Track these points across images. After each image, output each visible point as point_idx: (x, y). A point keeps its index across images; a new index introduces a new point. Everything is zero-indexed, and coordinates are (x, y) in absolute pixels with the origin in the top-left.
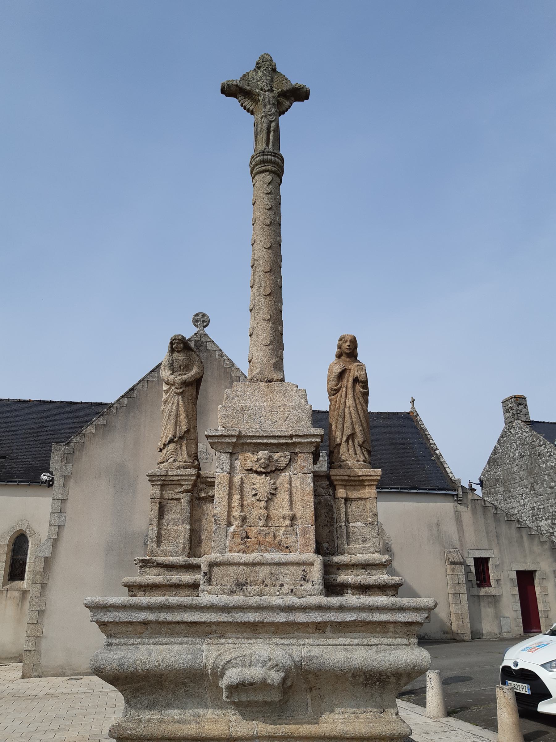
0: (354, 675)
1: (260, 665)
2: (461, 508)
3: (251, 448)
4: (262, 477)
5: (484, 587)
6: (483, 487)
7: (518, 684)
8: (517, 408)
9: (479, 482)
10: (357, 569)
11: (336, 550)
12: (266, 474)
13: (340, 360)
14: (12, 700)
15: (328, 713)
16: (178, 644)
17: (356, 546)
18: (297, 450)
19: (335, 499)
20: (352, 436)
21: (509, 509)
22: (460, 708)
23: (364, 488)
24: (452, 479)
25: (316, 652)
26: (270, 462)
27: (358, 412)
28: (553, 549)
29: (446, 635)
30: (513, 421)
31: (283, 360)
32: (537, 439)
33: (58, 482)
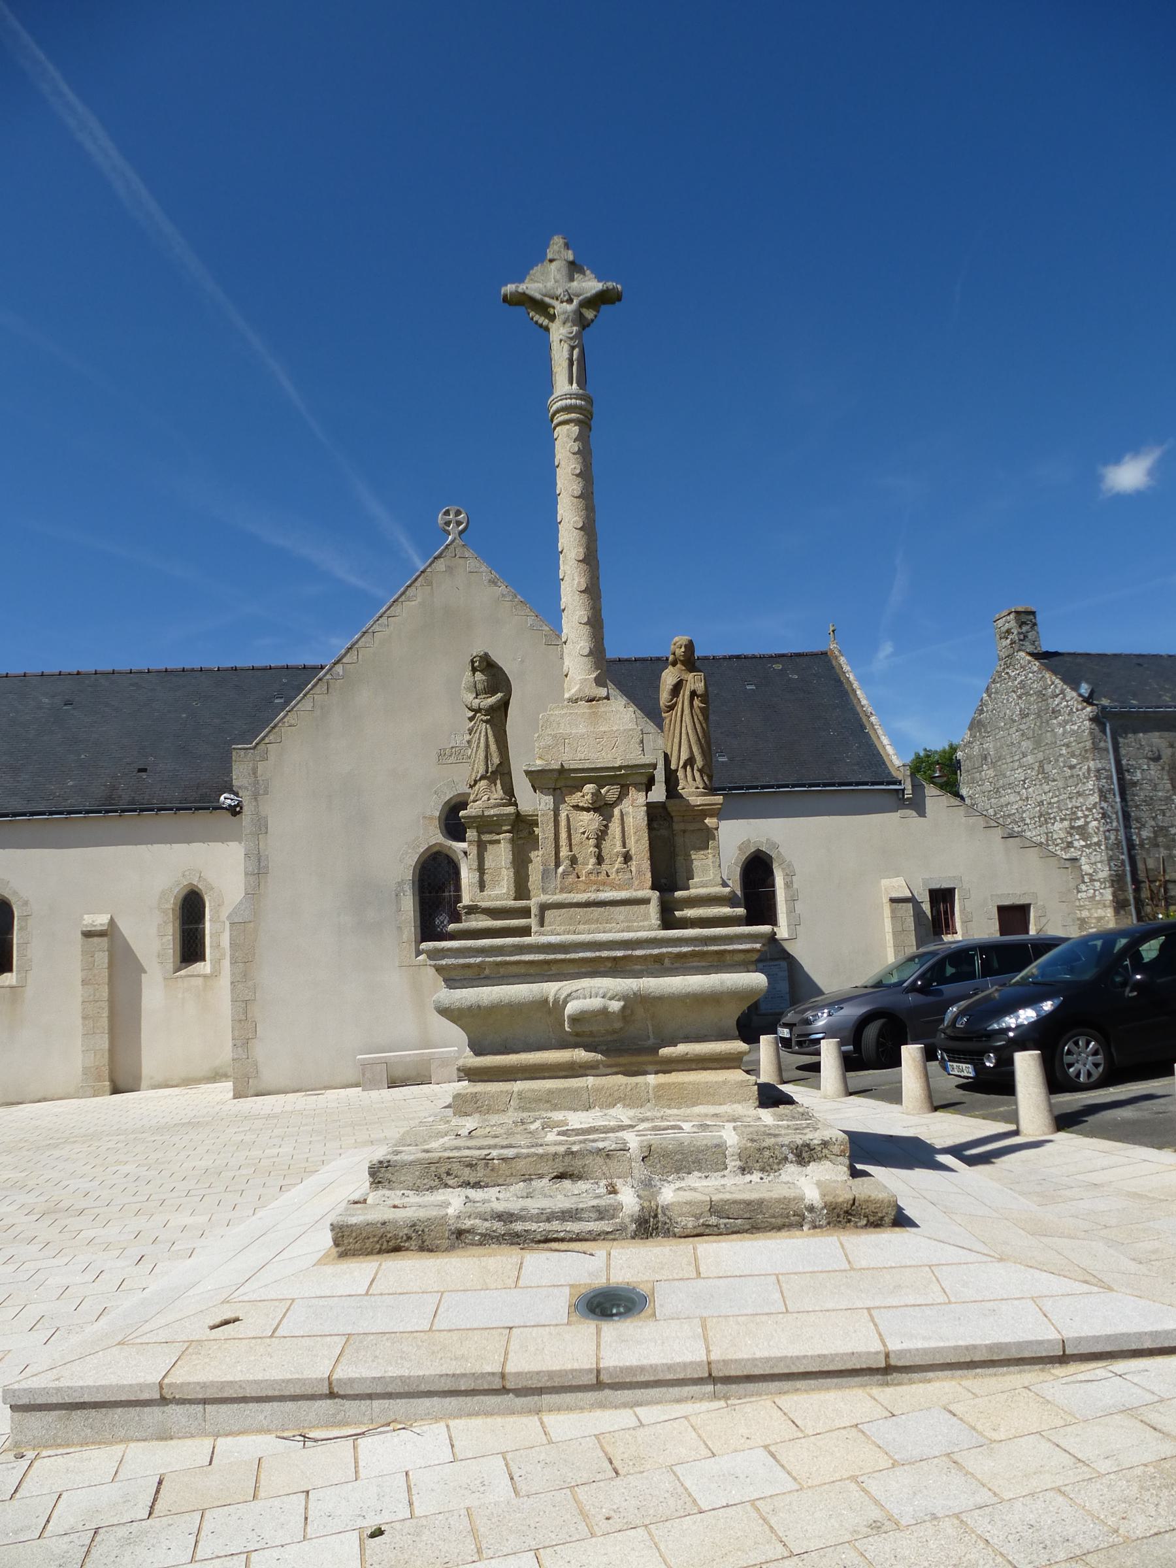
8: (1020, 630)
20: (690, 761)
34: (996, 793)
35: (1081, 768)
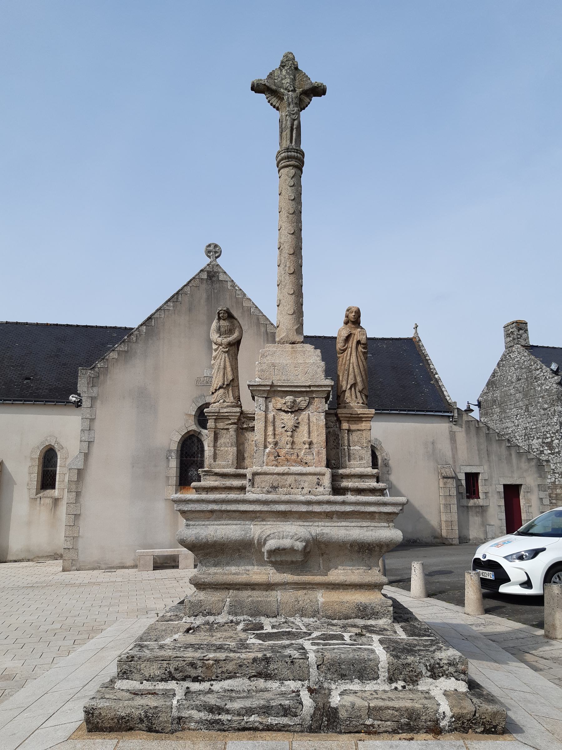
0: (351, 546)
1: (289, 538)
2: (456, 428)
3: (280, 394)
4: (289, 415)
5: (473, 498)
6: (480, 408)
7: (485, 572)
8: (518, 333)
9: (477, 404)
10: (355, 478)
11: (341, 465)
12: (292, 412)
13: (347, 326)
14: (62, 587)
15: (334, 569)
16: (234, 525)
17: (354, 463)
18: (314, 396)
19: (341, 430)
20: (354, 385)
21: (503, 429)
22: (439, 592)
23: (362, 423)
24: (449, 401)
25: (326, 530)
26: (294, 404)
27: (359, 367)
28: (539, 465)
29: (436, 540)
30: (513, 346)
31: (303, 325)
32: (534, 364)
33: (86, 403)
34: (500, 421)
35: (550, 410)
